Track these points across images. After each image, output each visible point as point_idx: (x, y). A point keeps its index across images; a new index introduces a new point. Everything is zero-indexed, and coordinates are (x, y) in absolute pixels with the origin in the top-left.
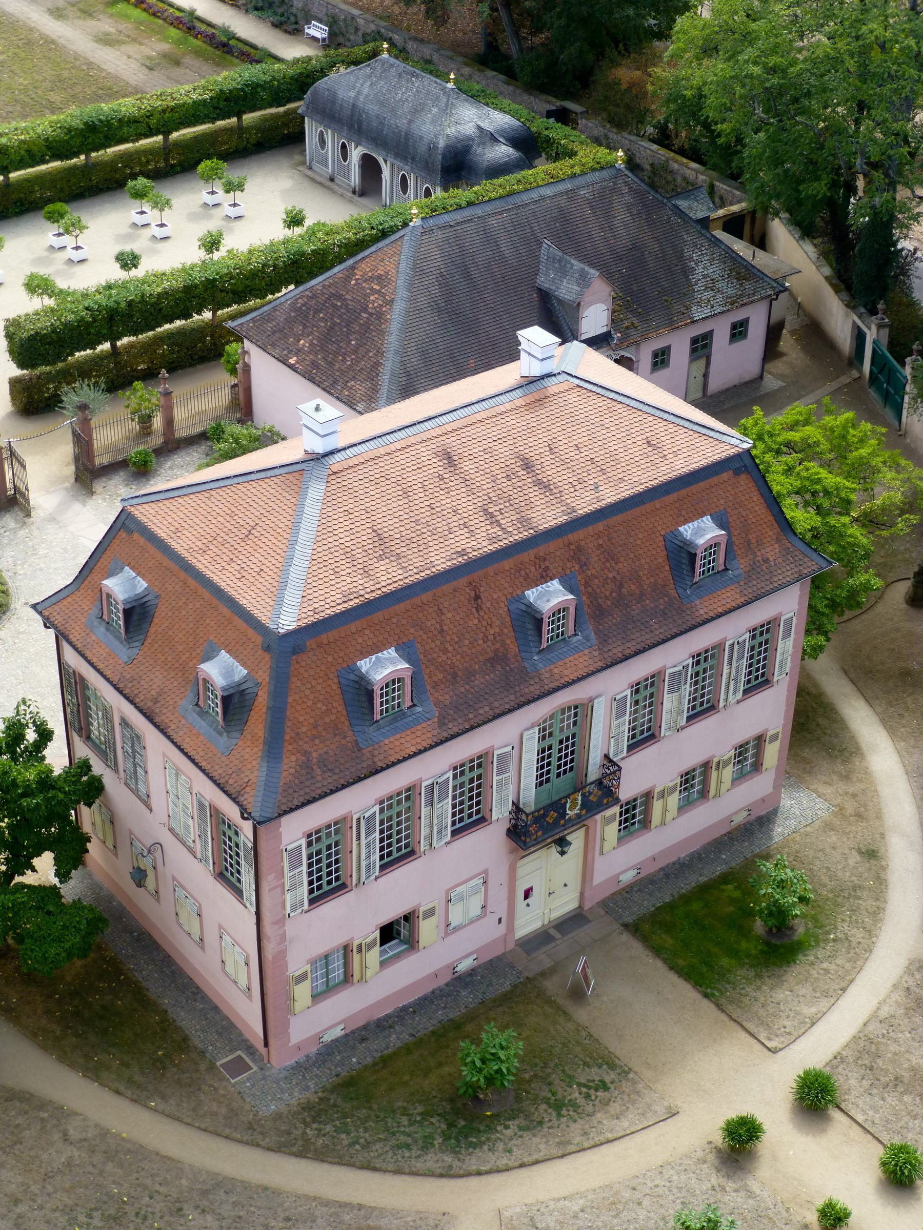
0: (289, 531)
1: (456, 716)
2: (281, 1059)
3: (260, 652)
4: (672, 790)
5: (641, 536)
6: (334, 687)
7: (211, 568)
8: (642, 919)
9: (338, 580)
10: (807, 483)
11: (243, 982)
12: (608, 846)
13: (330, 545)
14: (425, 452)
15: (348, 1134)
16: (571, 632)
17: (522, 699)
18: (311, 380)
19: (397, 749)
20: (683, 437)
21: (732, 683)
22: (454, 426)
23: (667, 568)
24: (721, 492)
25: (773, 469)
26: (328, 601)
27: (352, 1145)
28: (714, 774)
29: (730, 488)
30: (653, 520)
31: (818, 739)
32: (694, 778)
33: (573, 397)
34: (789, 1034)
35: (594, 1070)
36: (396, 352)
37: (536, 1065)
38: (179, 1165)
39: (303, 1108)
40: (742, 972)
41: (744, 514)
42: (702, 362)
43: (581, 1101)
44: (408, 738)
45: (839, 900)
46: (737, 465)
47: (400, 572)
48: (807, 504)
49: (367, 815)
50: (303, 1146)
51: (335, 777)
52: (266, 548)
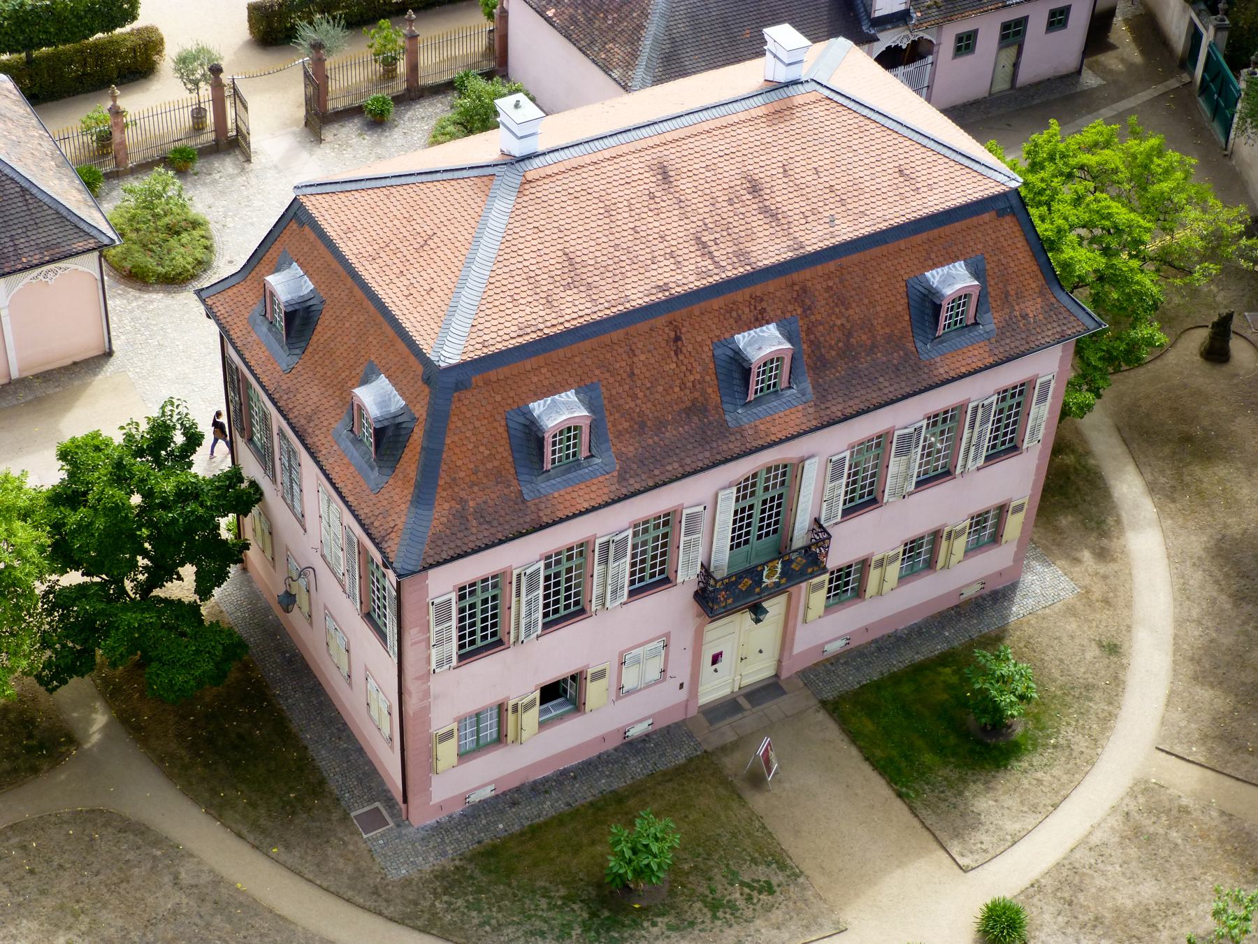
0: (467, 246)
1: (639, 471)
2: (421, 816)
3: (420, 383)
4: (893, 559)
5: (879, 280)
6: (501, 430)
7: (378, 279)
8: (842, 697)
9: (516, 310)
10: (1095, 217)
11: (386, 730)
12: (811, 615)
13: (512, 267)
14: (637, 165)
15: (480, 912)
16: (784, 384)
17: (719, 457)
18: (568, 37)
19: (568, 504)
20: (942, 169)
21: (973, 449)
22: (675, 135)
23: (907, 318)
24: (979, 235)
25: (1060, 197)
26: (501, 333)
27: (481, 925)
28: (944, 544)
29: (990, 232)
30: (896, 262)
31: (1076, 506)
32: (921, 546)
33: (819, 110)
34: (985, 851)
35: (762, 868)
36: (662, 16)
37: (699, 855)
38: (292, 927)
39: (436, 877)
40: (945, 772)
41: (1004, 261)
42: (1012, 51)
43: (741, 903)
44: (581, 493)
45: (1068, 699)
46: (1002, 205)
47: (589, 305)
48: (1093, 240)
49: (528, 572)
50: (429, 920)
51: (493, 531)
52: (440, 263)
